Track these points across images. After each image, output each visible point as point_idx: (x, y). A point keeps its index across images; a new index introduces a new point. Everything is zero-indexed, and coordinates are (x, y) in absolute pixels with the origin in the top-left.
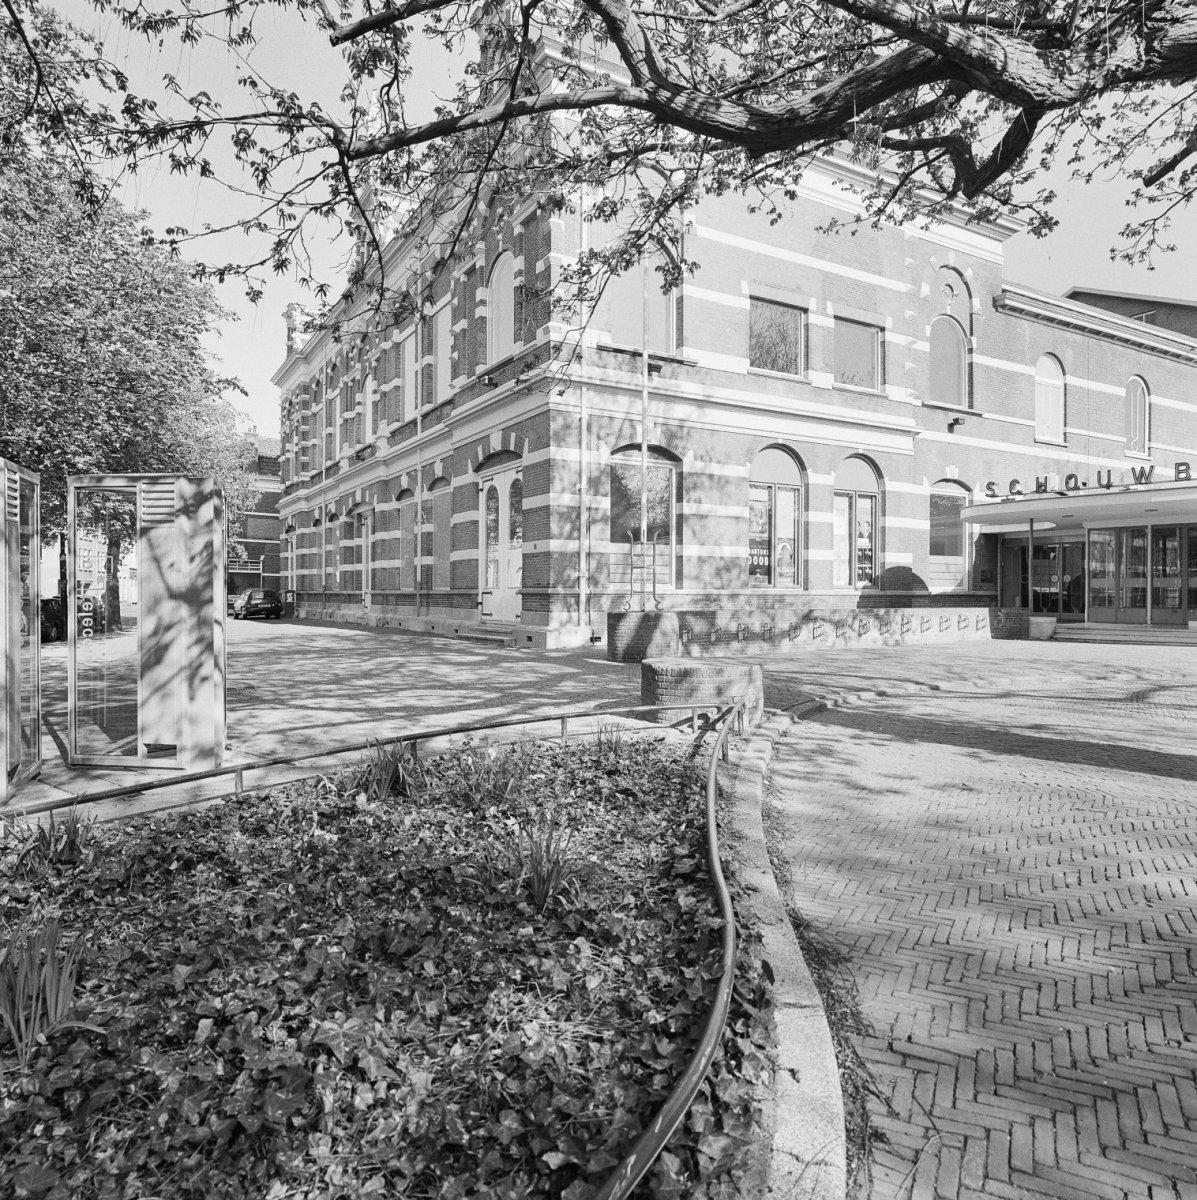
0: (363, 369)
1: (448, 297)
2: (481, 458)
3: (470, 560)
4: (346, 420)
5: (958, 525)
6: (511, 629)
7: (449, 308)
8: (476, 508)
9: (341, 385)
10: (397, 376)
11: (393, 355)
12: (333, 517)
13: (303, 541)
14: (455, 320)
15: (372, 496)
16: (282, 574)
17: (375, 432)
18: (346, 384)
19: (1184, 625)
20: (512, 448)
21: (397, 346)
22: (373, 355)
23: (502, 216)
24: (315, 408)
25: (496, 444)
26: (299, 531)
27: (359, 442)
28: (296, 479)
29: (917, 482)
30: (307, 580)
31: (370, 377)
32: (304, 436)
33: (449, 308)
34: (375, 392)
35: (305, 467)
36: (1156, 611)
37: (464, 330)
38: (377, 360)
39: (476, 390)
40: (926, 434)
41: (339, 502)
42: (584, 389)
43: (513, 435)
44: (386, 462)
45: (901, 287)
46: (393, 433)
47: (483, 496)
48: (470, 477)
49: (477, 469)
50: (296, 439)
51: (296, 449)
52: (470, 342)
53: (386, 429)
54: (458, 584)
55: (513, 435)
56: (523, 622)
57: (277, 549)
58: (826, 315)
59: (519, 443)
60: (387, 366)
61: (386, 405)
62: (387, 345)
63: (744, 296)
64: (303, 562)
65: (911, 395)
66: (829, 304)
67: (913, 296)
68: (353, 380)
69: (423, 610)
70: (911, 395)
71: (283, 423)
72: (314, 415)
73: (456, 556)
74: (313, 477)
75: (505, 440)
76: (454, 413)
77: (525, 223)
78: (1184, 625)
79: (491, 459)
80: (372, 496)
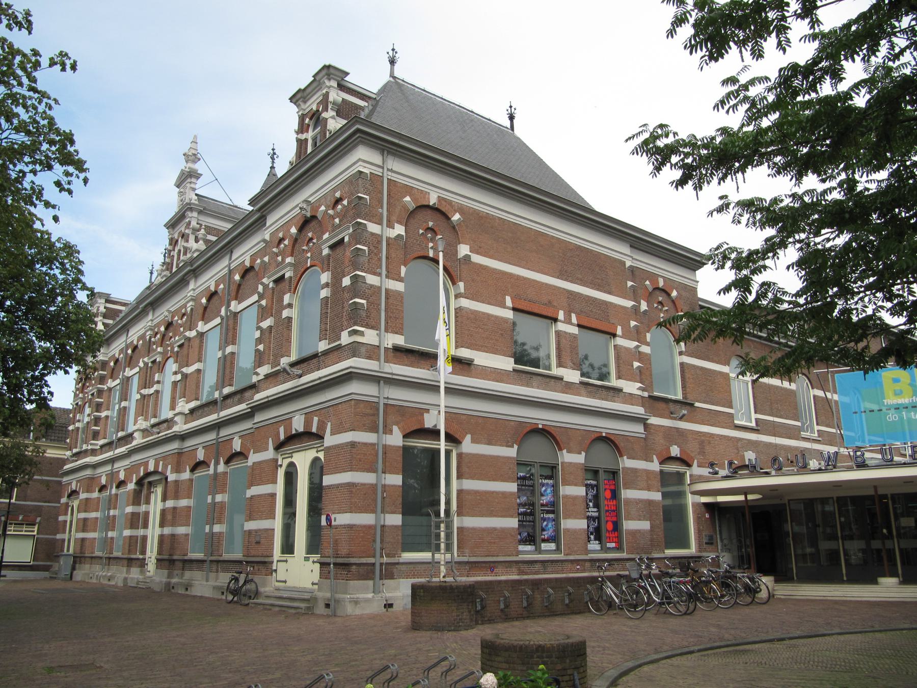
0: (164, 354)
1: (255, 298)
2: (282, 437)
3: (266, 530)
4: (143, 397)
5: (681, 495)
6: (307, 596)
7: (255, 307)
8: (274, 481)
9: (141, 364)
10: (200, 360)
11: (197, 341)
12: (121, 484)
13: (86, 505)
14: (262, 317)
15: (165, 467)
16: (59, 536)
17: (173, 408)
18: (146, 364)
19: (513, 447)
20: (314, 430)
21: (201, 335)
22: (178, 340)
23: (311, 239)
24: (111, 383)
25: (298, 425)
26: (83, 496)
27: (155, 417)
28: (85, 447)
29: (648, 459)
30: (87, 543)
31: (171, 360)
32: (98, 407)
33: (255, 307)
34: (175, 373)
35: (96, 435)
36: (891, 547)
37: (270, 327)
38: (181, 346)
39: (281, 378)
40: (654, 421)
41: (129, 471)
42: (382, 382)
43: (316, 419)
44: (183, 437)
45: (629, 304)
46: (192, 411)
47: (281, 473)
48: (270, 454)
49: (279, 447)
50: (88, 410)
51: (87, 419)
52: (275, 339)
53: (184, 406)
54: (253, 552)
55: (316, 419)
56: (319, 590)
57: (57, 512)
58: (572, 324)
59: (322, 426)
60: (190, 351)
61: (187, 386)
62: (192, 334)
63: (508, 308)
64: (84, 525)
65: (639, 389)
66: (574, 317)
67: (636, 309)
68: (154, 362)
69: (212, 575)
70: (639, 389)
71: (76, 395)
72: (110, 389)
73: (251, 525)
74: (102, 446)
75: (308, 423)
76: (258, 397)
77: (332, 247)
78: (513, 447)
79: (293, 439)
80: (165, 467)
